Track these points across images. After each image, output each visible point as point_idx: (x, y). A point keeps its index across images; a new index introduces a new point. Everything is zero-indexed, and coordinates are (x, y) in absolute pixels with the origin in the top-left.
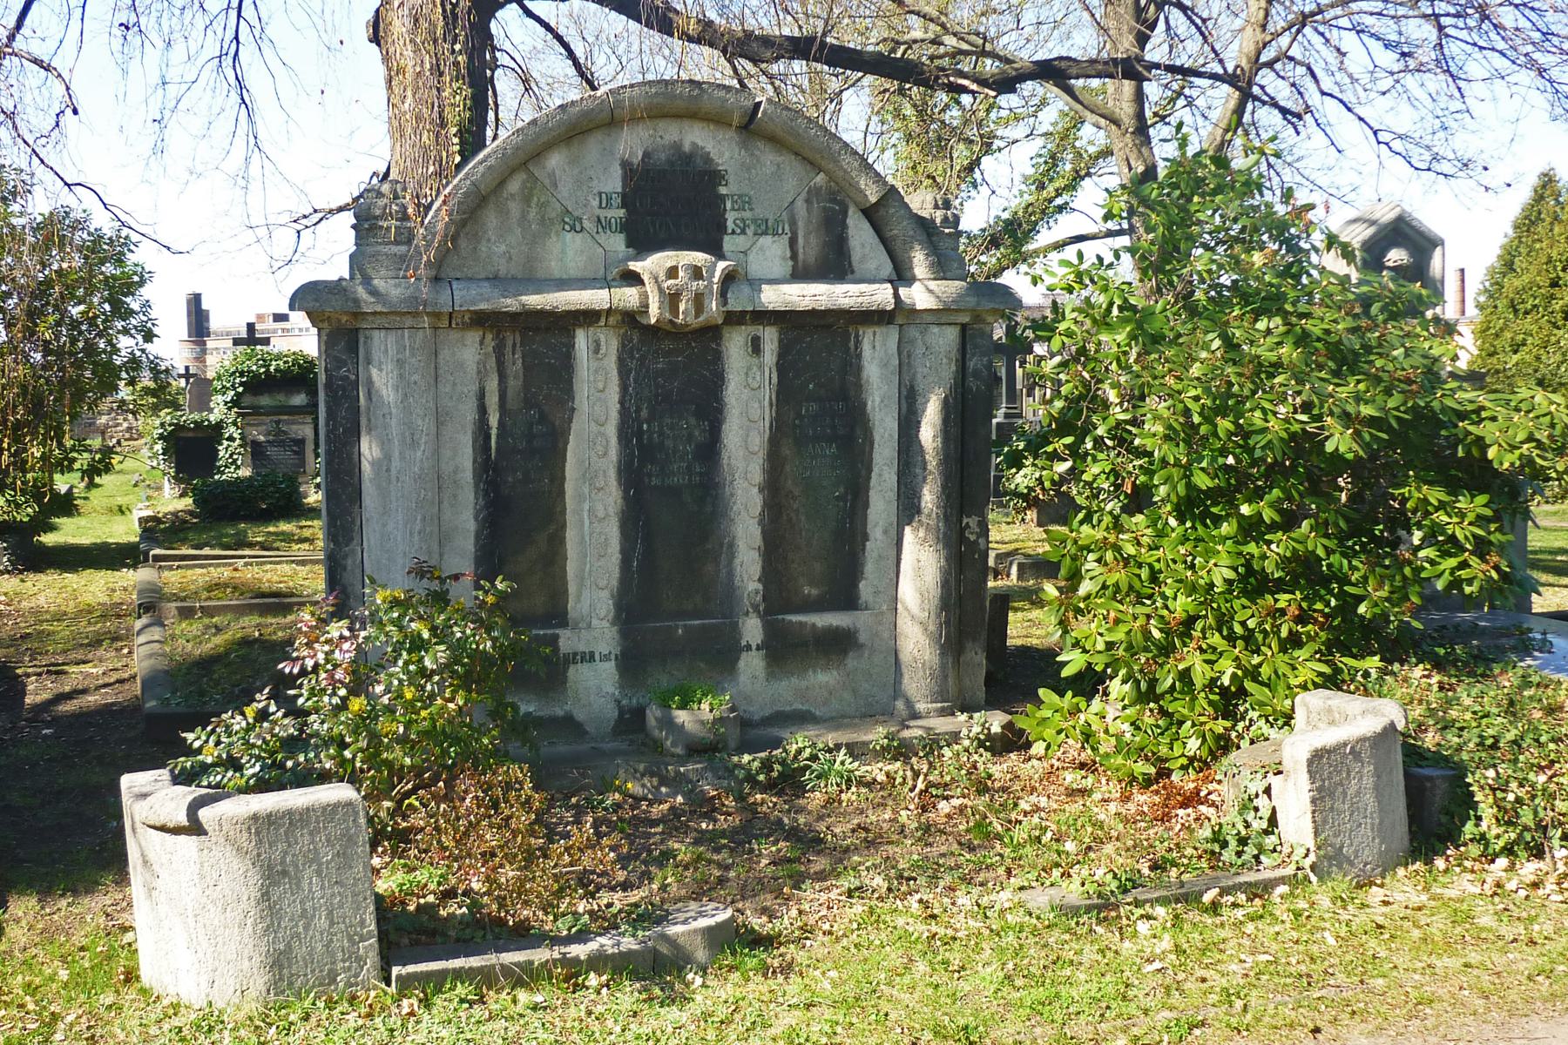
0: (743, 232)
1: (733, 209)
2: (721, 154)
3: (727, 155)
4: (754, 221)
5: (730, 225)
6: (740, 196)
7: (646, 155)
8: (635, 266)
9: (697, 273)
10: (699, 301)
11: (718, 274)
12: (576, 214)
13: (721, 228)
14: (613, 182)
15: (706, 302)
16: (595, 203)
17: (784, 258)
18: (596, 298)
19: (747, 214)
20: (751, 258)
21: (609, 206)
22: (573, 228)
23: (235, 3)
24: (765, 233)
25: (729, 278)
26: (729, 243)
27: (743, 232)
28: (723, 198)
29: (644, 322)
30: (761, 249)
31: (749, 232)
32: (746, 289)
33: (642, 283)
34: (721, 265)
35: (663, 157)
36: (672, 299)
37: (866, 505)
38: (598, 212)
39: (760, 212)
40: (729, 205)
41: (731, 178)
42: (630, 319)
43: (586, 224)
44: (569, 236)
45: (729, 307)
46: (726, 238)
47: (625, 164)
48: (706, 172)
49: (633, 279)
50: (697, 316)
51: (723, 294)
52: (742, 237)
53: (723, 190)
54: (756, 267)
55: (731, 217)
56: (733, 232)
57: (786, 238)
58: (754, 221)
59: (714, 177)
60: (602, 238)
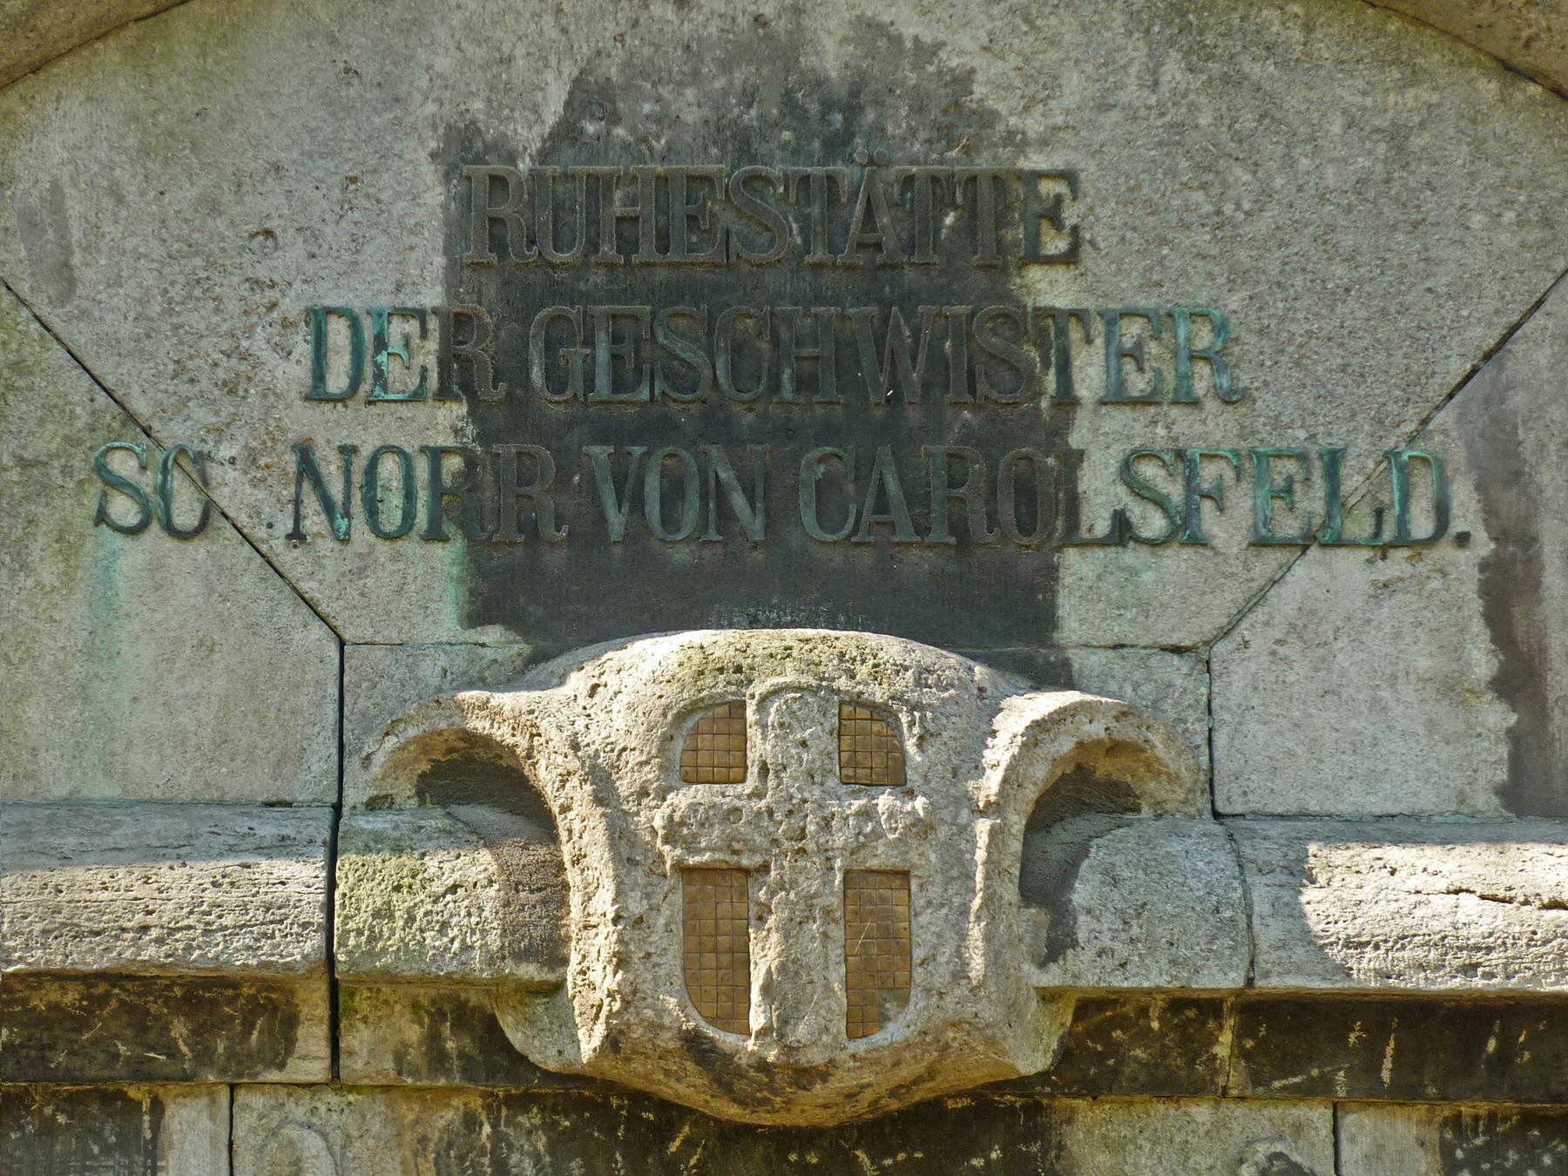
0: (1185, 531)
1: (1117, 397)
2: (1040, 87)
3: (1075, 87)
4: (1253, 463)
5: (1100, 491)
6: (1159, 322)
7: (589, 96)
8: (499, 714)
9: (866, 744)
10: (873, 898)
11: (999, 753)
12: (175, 432)
13: (1042, 502)
14: (405, 260)
15: (926, 927)
16: (294, 371)
17: (1452, 688)
18: (248, 904)
19: (1211, 427)
20: (1239, 677)
21: (366, 385)
22: (156, 514)
23: (245, 1162)
24: (1322, 537)
25: (1082, 794)
26: (1088, 595)
27: (1185, 531)
28: (1052, 331)
29: (544, 1055)
30: (1303, 629)
31: (1225, 529)
32: (1200, 859)
33: (537, 817)
34: (1027, 708)
35: (690, 109)
36: (709, 896)
37: (503, 691)
38: (305, 420)
39: (1286, 413)
40: (1090, 376)
41: (1097, 214)
42: (473, 1033)
43: (231, 488)
44: (133, 556)
45: (1086, 970)
46: (1077, 566)
47: (463, 150)
48: (941, 188)
49: (480, 784)
50: (861, 1020)
51: (1043, 887)
52: (1178, 559)
53: (1050, 289)
54: (1269, 737)
55: (1101, 443)
56: (1122, 531)
57: (1465, 566)
58: (1253, 463)
59: (988, 214)
60: (321, 568)
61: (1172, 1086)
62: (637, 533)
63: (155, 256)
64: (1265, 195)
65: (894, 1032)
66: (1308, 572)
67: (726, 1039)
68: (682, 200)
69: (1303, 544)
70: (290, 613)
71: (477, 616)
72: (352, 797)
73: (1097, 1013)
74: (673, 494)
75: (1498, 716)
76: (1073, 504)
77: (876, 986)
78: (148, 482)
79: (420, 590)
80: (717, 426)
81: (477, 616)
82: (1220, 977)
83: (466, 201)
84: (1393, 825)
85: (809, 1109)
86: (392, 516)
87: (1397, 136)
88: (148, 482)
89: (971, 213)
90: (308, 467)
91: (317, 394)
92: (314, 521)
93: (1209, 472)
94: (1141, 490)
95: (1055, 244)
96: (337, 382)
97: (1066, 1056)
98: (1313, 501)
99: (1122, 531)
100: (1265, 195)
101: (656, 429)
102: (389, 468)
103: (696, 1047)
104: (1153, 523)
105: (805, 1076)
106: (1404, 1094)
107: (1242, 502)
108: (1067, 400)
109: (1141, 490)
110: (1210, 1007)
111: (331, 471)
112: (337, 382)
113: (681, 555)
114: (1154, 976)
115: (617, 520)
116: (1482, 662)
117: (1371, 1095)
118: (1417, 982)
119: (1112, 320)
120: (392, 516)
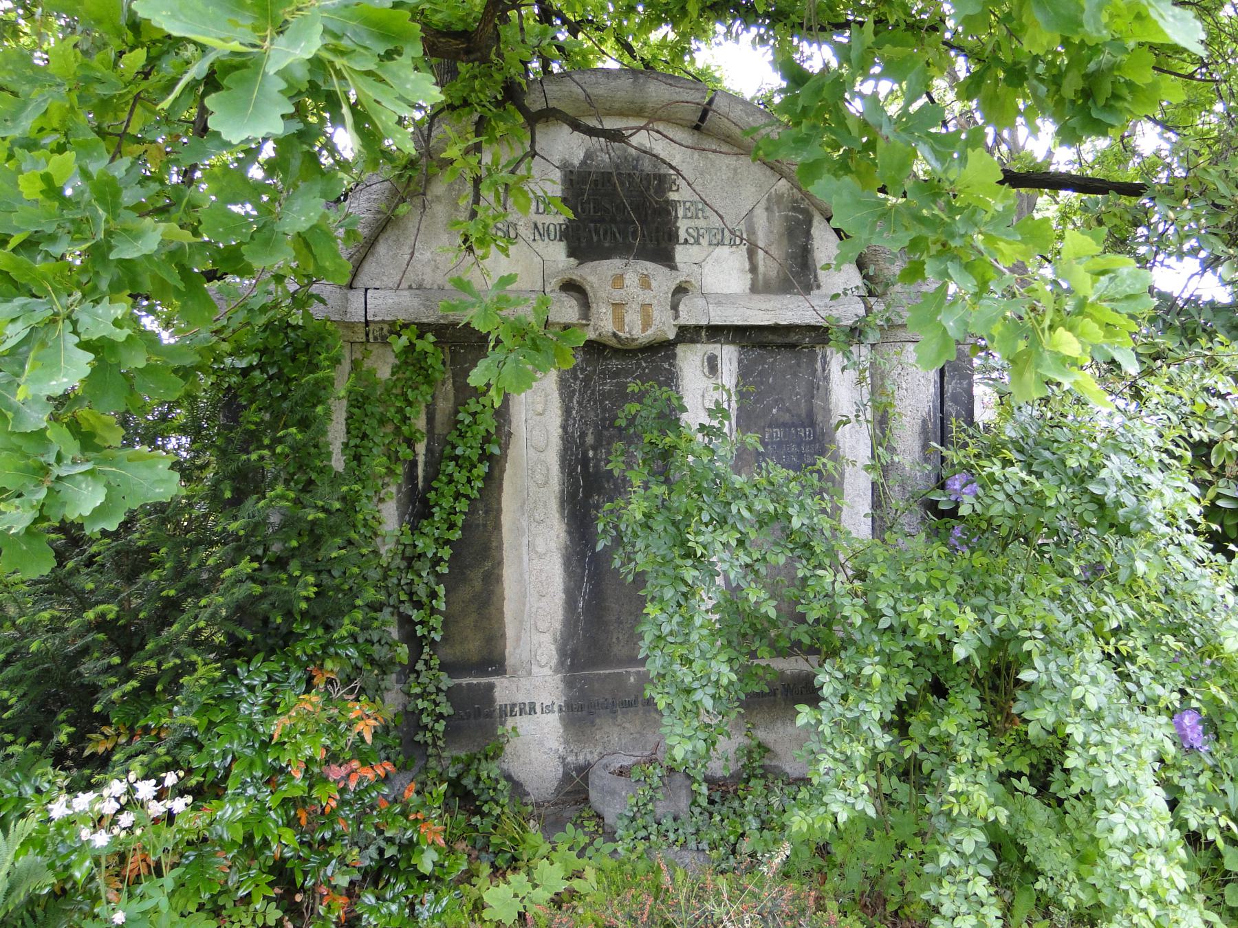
0: (697, 242)
1: (685, 217)
4: (708, 230)
5: (682, 234)
17: (743, 271)
19: (701, 223)
25: (681, 290)
27: (697, 242)
28: (674, 204)
31: (704, 242)
32: (700, 302)
40: (680, 213)
45: (683, 320)
50: (643, 331)
51: (675, 307)
52: (696, 247)
55: (683, 226)
56: (686, 241)
60: (540, 246)
61: (693, 341)
62: (599, 240)
63: (502, 358)
64: (712, 180)
65: (649, 332)
66: (719, 250)
67: (620, 334)
68: (606, 177)
69: (717, 245)
70: (534, 255)
71: (569, 256)
72: (547, 290)
73: (683, 329)
74: (606, 233)
75: (749, 276)
76: (677, 237)
77: (646, 325)
78: (505, 229)
79: (557, 254)
80: (613, 220)
81: (569, 256)
82: (704, 322)
83: (565, 176)
84: (779, 340)
85: (634, 345)
86: (552, 237)
87: (735, 170)
88: (505, 229)
89: (660, 181)
90: (536, 227)
91: (537, 212)
92: (537, 237)
93: (701, 231)
94: (689, 234)
95: (674, 188)
96: (541, 211)
97: (677, 335)
98: (719, 237)
99: (686, 241)
100: (712, 180)
101: (602, 220)
102: (552, 227)
103: (615, 335)
104: (691, 241)
105: (633, 340)
106: (733, 342)
107: (706, 237)
108: (677, 217)
109: (689, 234)
110: (701, 327)
111: (540, 227)
112: (541, 211)
113: (607, 245)
114: (693, 322)
115: (595, 239)
116: (747, 266)
117: (728, 343)
118: (736, 323)
119: (685, 203)
120: (552, 237)
